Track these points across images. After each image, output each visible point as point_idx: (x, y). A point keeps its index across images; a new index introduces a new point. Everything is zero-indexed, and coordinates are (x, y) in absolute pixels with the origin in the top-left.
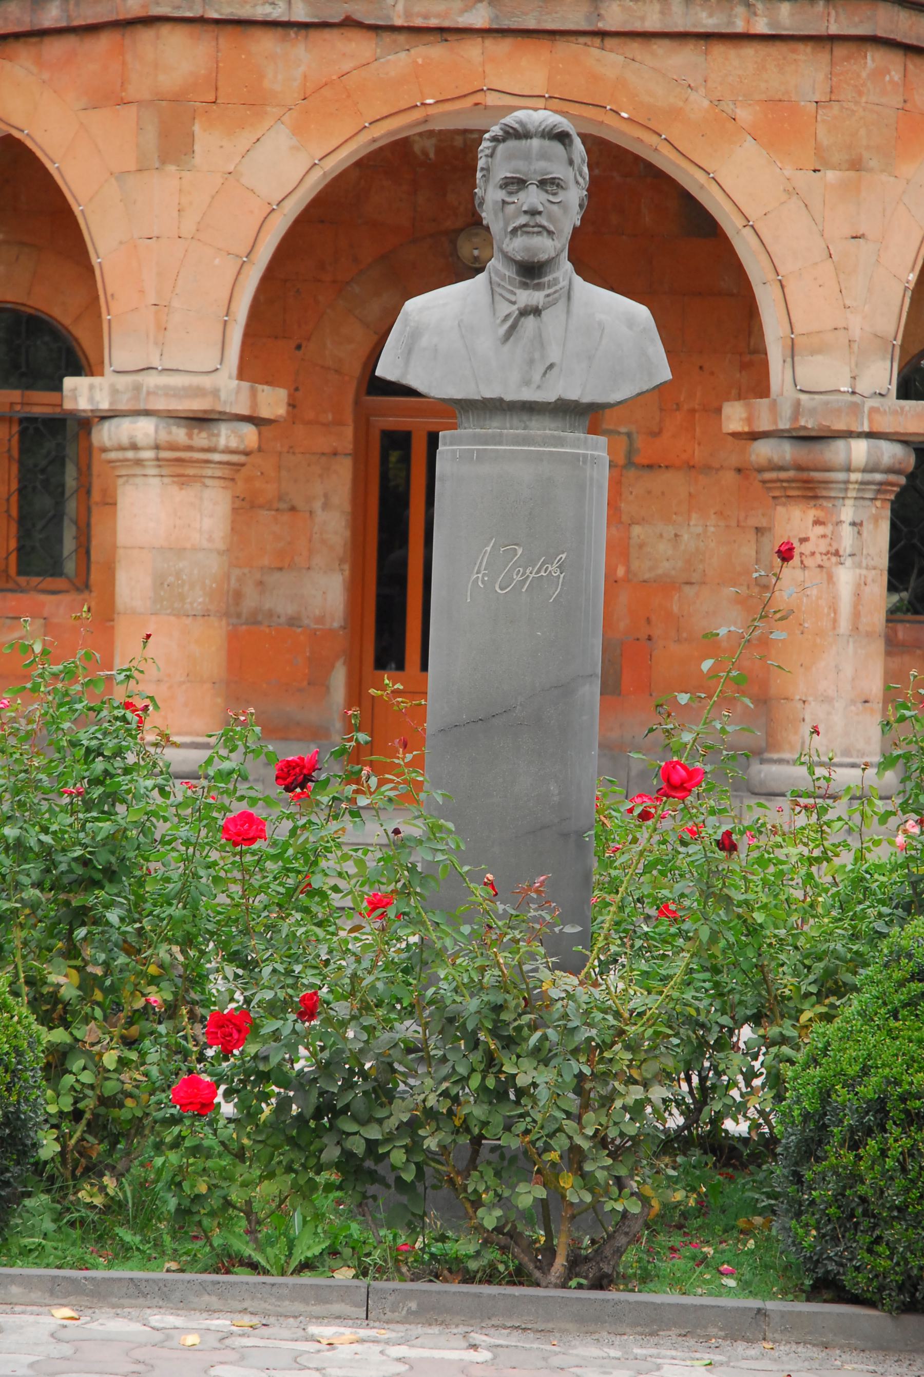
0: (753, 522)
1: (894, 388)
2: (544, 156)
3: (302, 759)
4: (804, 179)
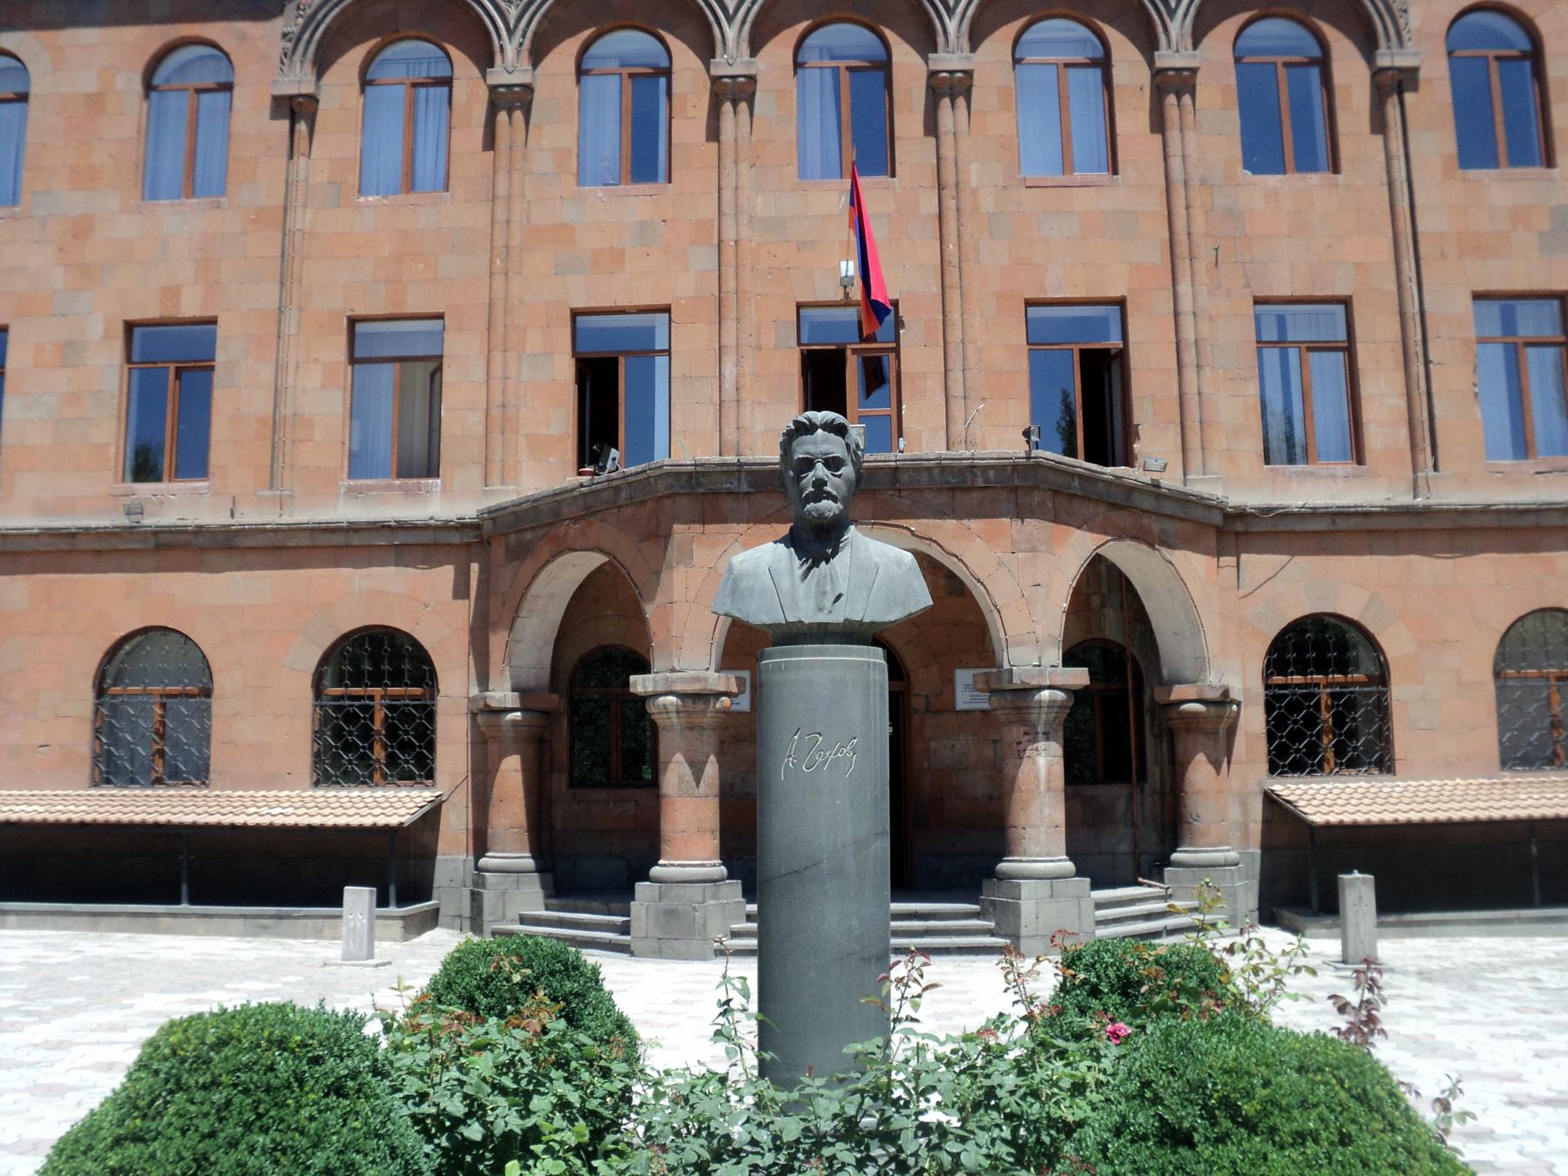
2: (825, 441)
3: (114, 1091)
4: (1007, 557)
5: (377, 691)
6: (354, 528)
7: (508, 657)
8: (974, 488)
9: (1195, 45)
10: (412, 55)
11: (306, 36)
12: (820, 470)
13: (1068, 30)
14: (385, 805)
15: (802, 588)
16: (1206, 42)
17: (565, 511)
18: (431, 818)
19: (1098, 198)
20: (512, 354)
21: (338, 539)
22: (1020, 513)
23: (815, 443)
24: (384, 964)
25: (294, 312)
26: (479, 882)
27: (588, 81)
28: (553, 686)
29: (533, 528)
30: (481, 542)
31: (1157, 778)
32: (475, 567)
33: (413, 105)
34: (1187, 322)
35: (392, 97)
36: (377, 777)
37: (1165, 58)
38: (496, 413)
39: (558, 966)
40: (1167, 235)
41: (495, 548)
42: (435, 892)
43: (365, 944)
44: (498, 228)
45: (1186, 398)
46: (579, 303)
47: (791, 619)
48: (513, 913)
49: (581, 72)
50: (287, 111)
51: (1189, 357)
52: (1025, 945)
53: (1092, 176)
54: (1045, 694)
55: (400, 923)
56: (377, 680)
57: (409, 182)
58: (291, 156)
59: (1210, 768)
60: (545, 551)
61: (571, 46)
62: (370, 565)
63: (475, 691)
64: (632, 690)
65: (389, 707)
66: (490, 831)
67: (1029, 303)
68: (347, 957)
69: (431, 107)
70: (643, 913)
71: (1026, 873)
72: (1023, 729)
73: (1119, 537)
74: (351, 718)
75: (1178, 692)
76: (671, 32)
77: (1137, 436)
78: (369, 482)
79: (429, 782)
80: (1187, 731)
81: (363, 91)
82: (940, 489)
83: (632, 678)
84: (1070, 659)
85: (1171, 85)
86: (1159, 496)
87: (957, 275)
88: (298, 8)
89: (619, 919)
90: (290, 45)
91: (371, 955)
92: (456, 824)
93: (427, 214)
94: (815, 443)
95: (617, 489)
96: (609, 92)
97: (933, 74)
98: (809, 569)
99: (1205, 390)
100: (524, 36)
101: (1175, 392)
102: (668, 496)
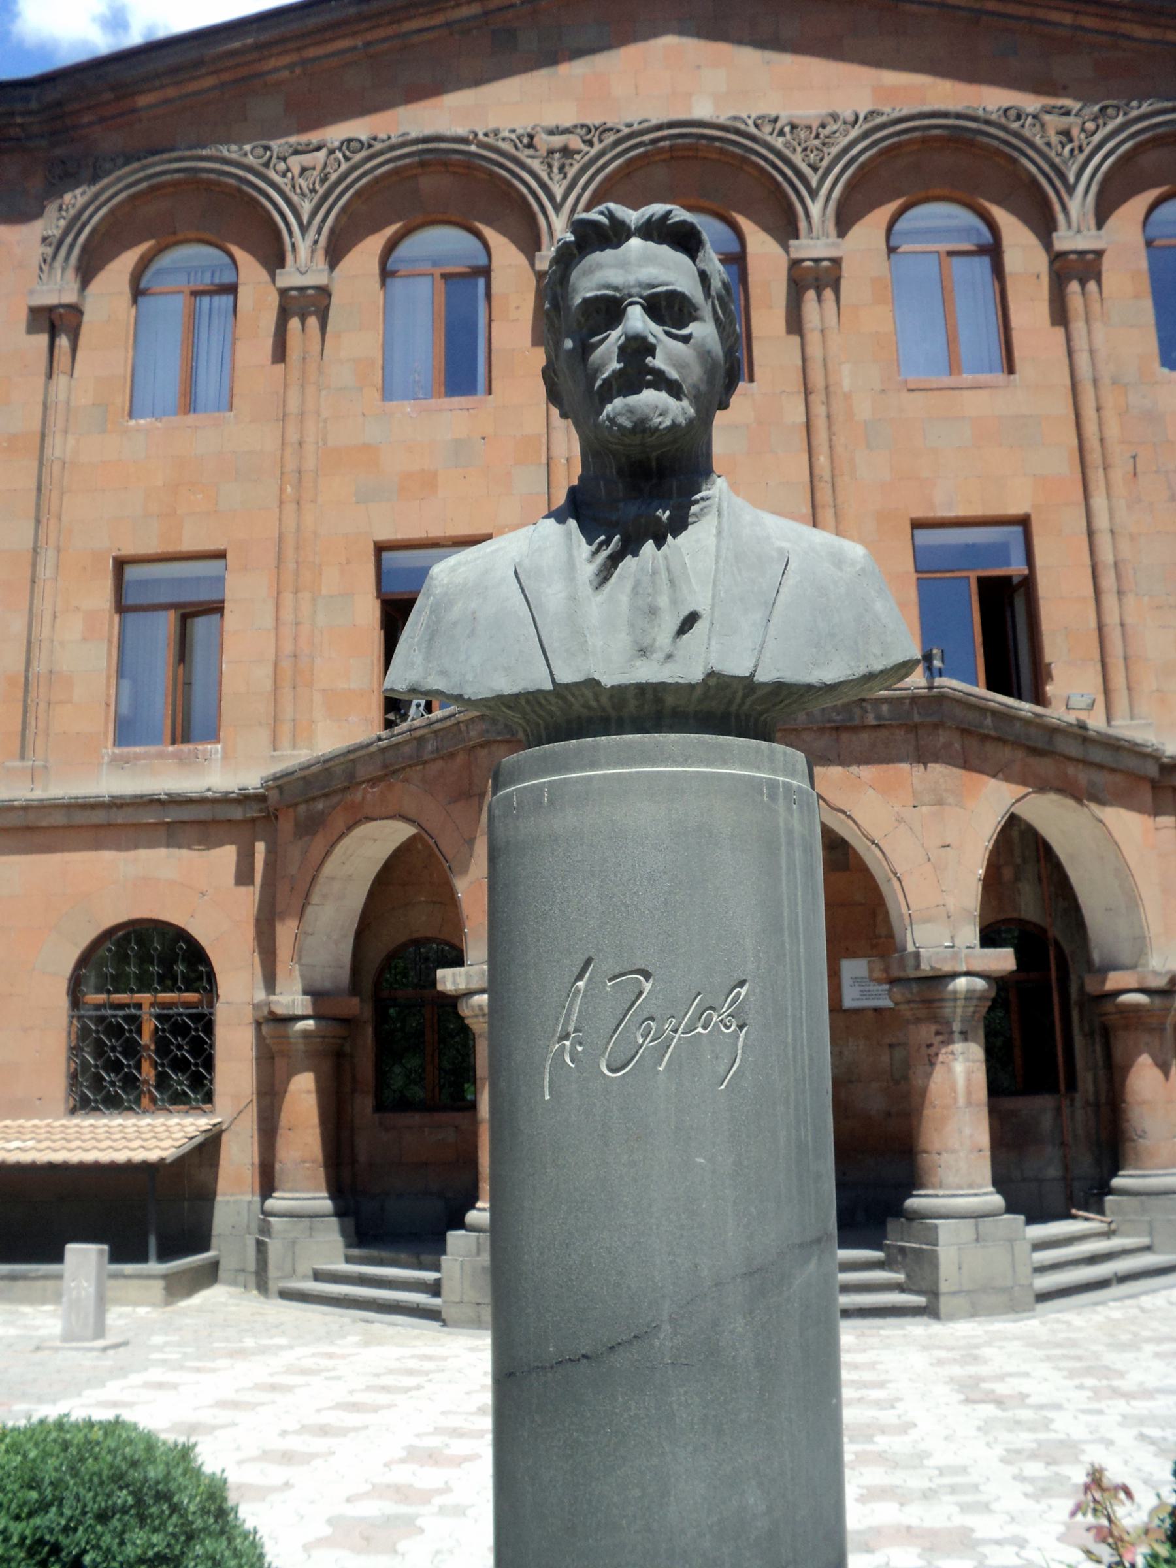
0: (887, 1041)
1: (977, 942)
2: (646, 260)
5: (145, 997)
6: (117, 804)
7: (298, 954)
8: (865, 727)
9: (1100, 225)
10: (193, 258)
11: (69, 240)
12: (636, 319)
13: (949, 216)
14: (148, 1136)
15: (595, 605)
16: (1113, 222)
17: (363, 772)
18: (208, 1149)
19: (988, 400)
20: (306, 595)
21: (99, 817)
22: (922, 757)
23: (624, 265)
24: (116, 1346)
25: (51, 553)
26: (265, 1229)
27: (396, 284)
28: (355, 987)
29: (326, 795)
30: (267, 818)
31: (1091, 1088)
32: (260, 847)
33: (193, 318)
34: (1104, 542)
35: (170, 308)
36: (145, 1101)
37: (1064, 240)
38: (286, 664)
39: (123, 1497)
40: (1076, 442)
41: (283, 821)
42: (214, 1242)
43: (91, 1320)
44: (289, 451)
45: (1106, 630)
46: (386, 534)
47: (567, 675)
48: (305, 1267)
49: (386, 274)
50: (47, 324)
51: (1108, 581)
52: (945, 1304)
53: (984, 378)
54: (962, 983)
55: (159, 1284)
56: (144, 985)
57: (189, 402)
58: (50, 375)
59: (1157, 1073)
60: (339, 821)
61: (374, 244)
62: (136, 847)
63: (260, 995)
64: (440, 987)
65: (159, 1017)
66: (278, 1166)
67: (917, 525)
68: (69, 1336)
69: (215, 321)
70: (457, 1266)
71: (943, 1211)
72: (933, 1028)
73: (1042, 787)
74: (115, 1031)
75: (1114, 981)
76: (489, 224)
77: (1050, 676)
78: (137, 749)
79: (207, 1107)
80: (1126, 1027)
81: (135, 301)
82: (822, 730)
83: (440, 973)
84: (989, 938)
85: (1072, 271)
86: (1085, 740)
87: (830, 492)
88: (60, 209)
89: (429, 1276)
90: (49, 251)
91: (100, 1330)
92: (239, 1157)
93: (204, 437)
94: (624, 265)
95: (421, 740)
96: (422, 298)
97: (795, 264)
98: (614, 560)
99: (1129, 620)
100: (319, 232)
101: (1093, 624)
102: (482, 746)
